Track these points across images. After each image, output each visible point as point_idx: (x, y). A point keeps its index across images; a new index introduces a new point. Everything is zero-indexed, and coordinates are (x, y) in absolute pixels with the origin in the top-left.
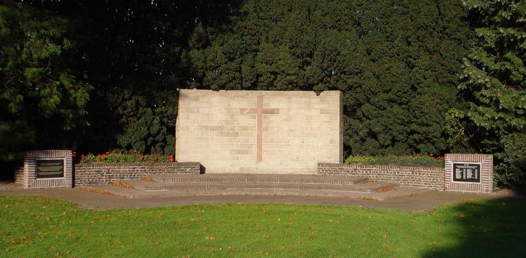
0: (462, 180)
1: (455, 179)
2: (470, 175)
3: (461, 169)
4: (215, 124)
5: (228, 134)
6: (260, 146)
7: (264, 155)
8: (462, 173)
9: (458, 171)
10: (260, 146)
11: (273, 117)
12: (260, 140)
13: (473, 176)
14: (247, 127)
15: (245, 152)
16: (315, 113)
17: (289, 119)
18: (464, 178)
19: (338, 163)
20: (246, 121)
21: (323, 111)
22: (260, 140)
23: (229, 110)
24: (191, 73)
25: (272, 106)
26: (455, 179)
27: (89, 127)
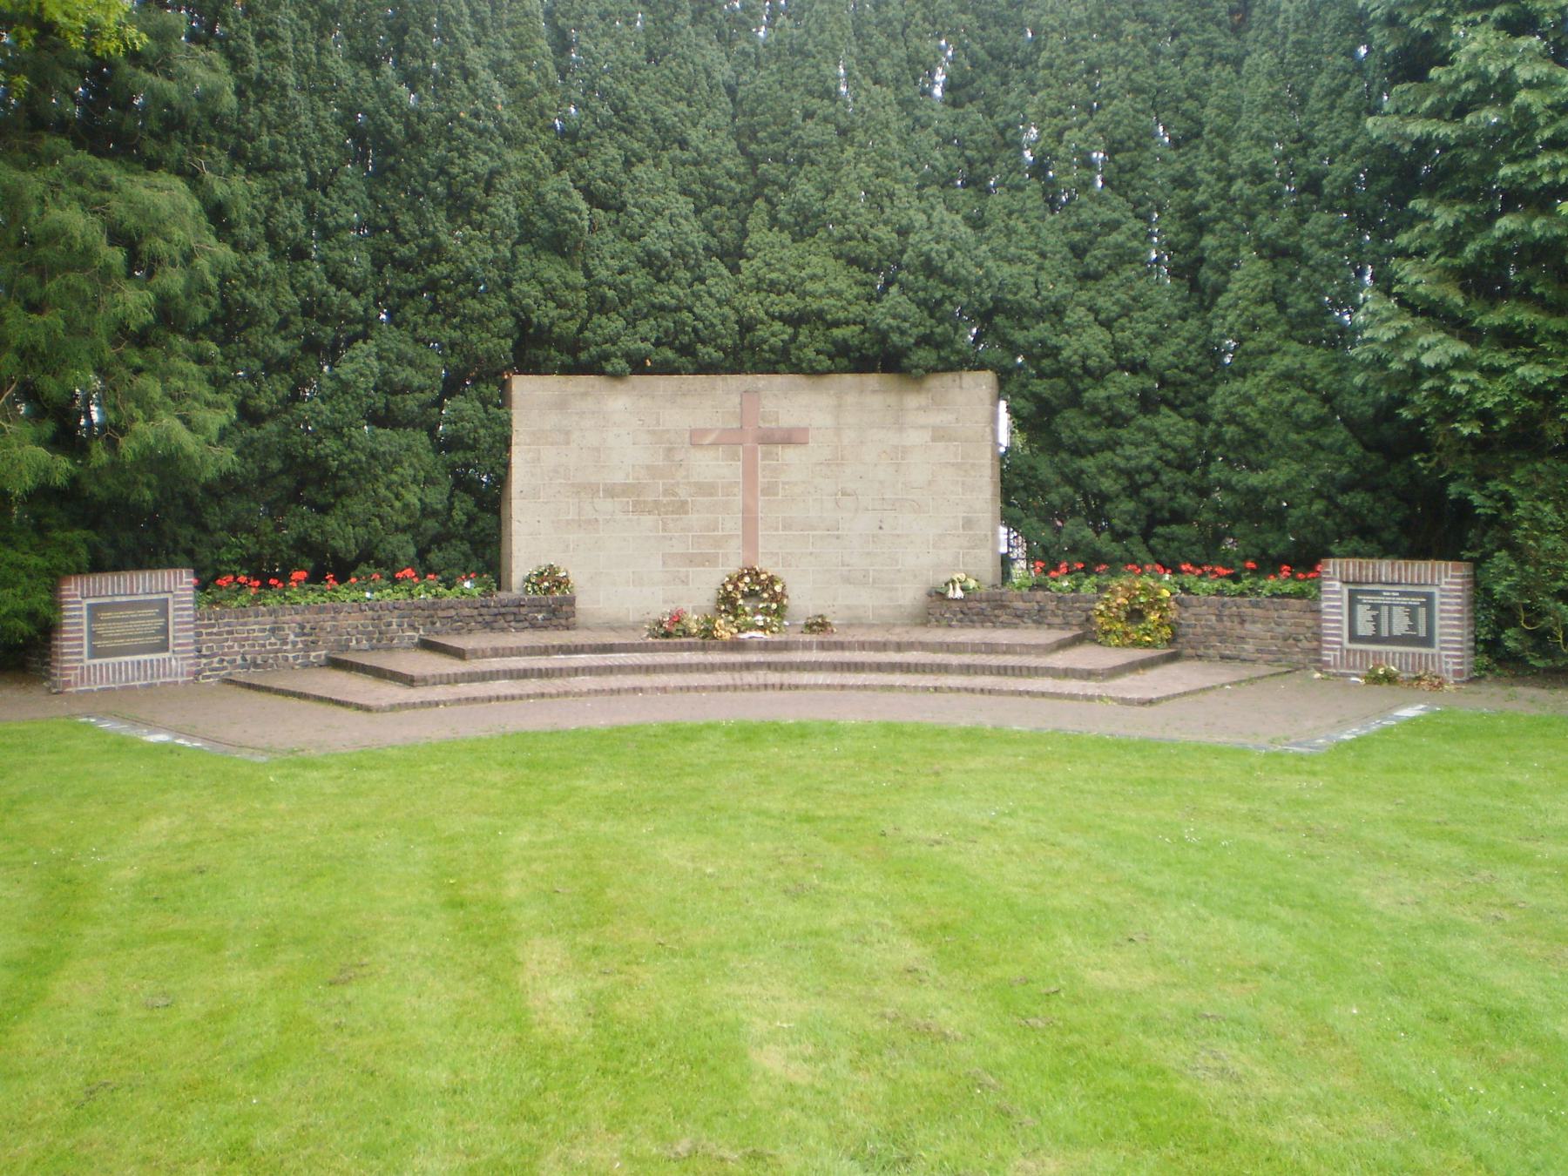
0: (1375, 639)
3: (1374, 607)
4: (619, 478)
8: (1376, 619)
9: (1363, 614)
11: (789, 454)
13: (1413, 627)
20: (710, 465)
26: (1354, 637)
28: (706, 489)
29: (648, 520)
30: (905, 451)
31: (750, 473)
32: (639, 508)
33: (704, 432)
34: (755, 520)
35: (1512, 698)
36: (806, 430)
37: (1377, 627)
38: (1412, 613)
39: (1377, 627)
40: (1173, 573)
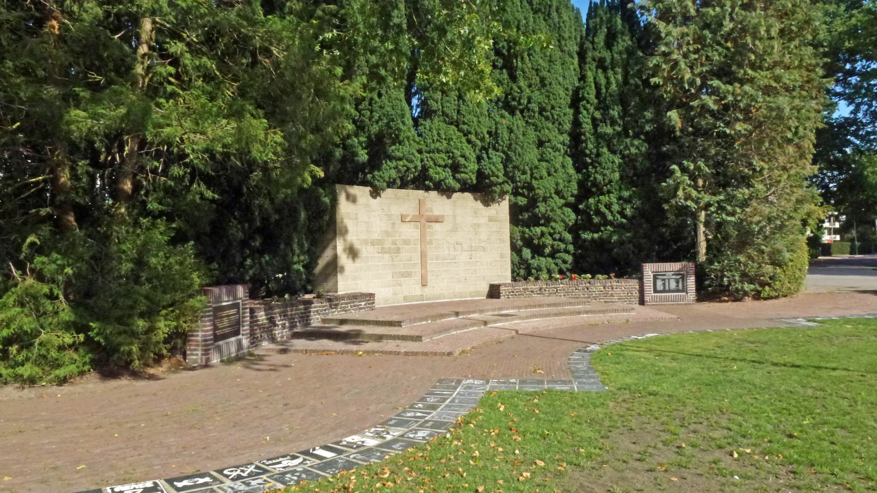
0: (664, 291)
1: (655, 291)
2: (673, 285)
3: (663, 280)
4: (375, 236)
5: (389, 251)
6: (424, 264)
7: (430, 277)
8: (664, 284)
9: (659, 284)
10: (424, 264)
11: (437, 226)
12: (423, 255)
13: (677, 286)
14: (409, 240)
15: (408, 275)
16: (483, 220)
17: (455, 229)
18: (667, 288)
19: (510, 281)
20: (410, 231)
21: (491, 219)
22: (423, 255)
23: (389, 216)
24: (504, 71)
25: (436, 212)
26: (655, 291)
27: (3, 478)
28: (406, 242)
29: (387, 256)
30: (479, 225)
31: (423, 236)
32: (383, 251)
33: (407, 216)
34: (426, 255)
35: (405, 298)
36: (443, 216)
37: (664, 287)
38: (677, 282)
39: (664, 287)
40: (258, 228)
